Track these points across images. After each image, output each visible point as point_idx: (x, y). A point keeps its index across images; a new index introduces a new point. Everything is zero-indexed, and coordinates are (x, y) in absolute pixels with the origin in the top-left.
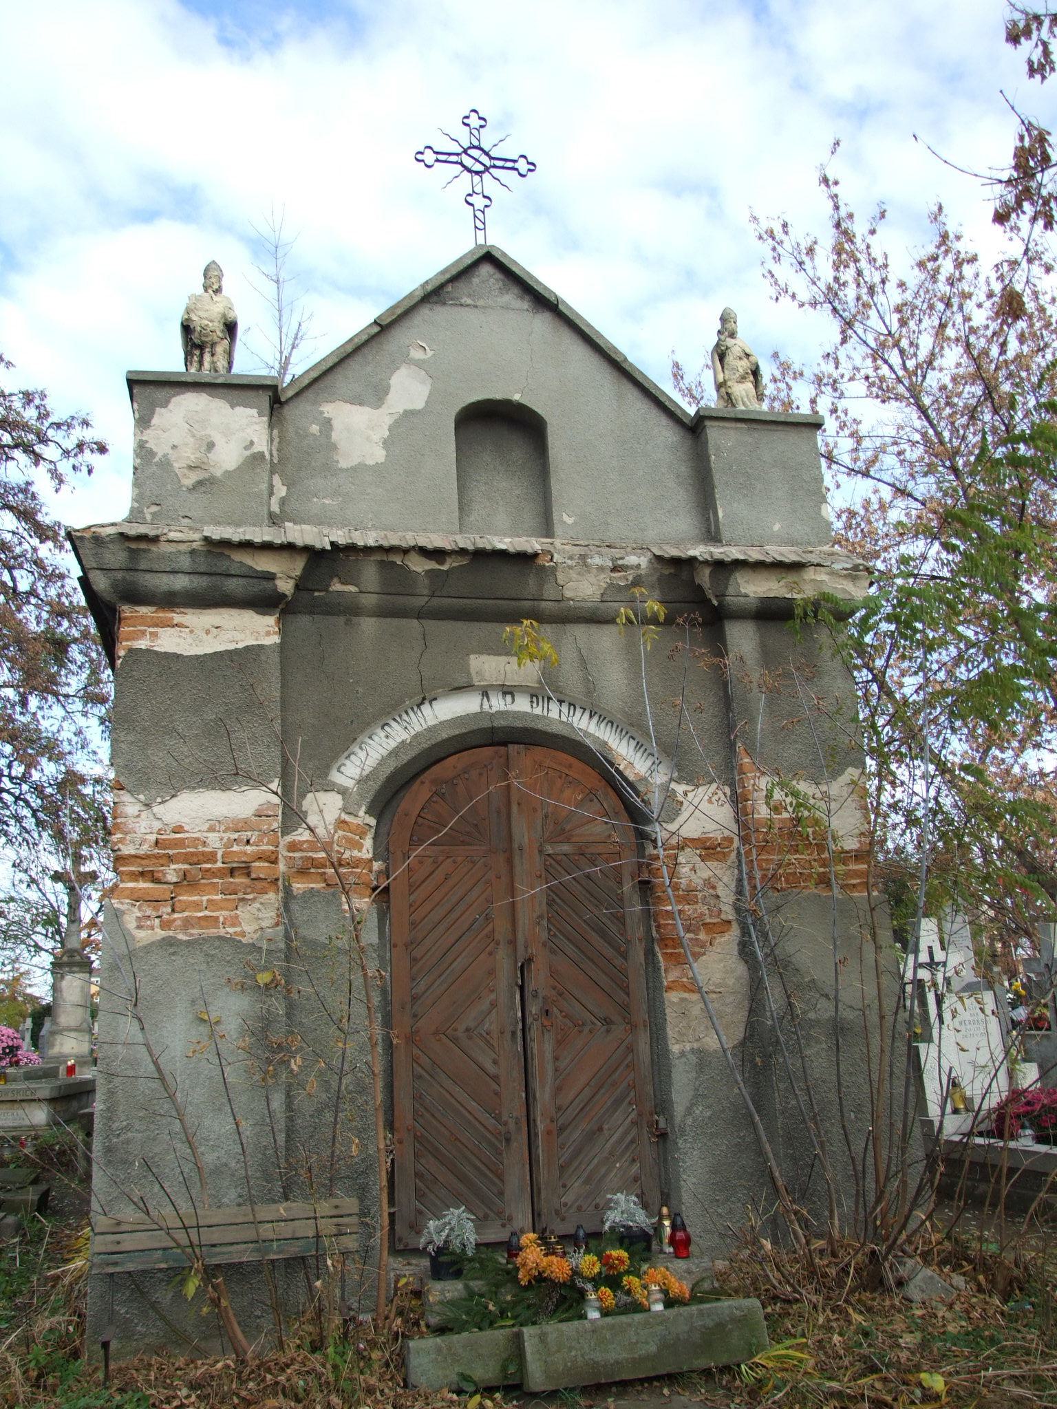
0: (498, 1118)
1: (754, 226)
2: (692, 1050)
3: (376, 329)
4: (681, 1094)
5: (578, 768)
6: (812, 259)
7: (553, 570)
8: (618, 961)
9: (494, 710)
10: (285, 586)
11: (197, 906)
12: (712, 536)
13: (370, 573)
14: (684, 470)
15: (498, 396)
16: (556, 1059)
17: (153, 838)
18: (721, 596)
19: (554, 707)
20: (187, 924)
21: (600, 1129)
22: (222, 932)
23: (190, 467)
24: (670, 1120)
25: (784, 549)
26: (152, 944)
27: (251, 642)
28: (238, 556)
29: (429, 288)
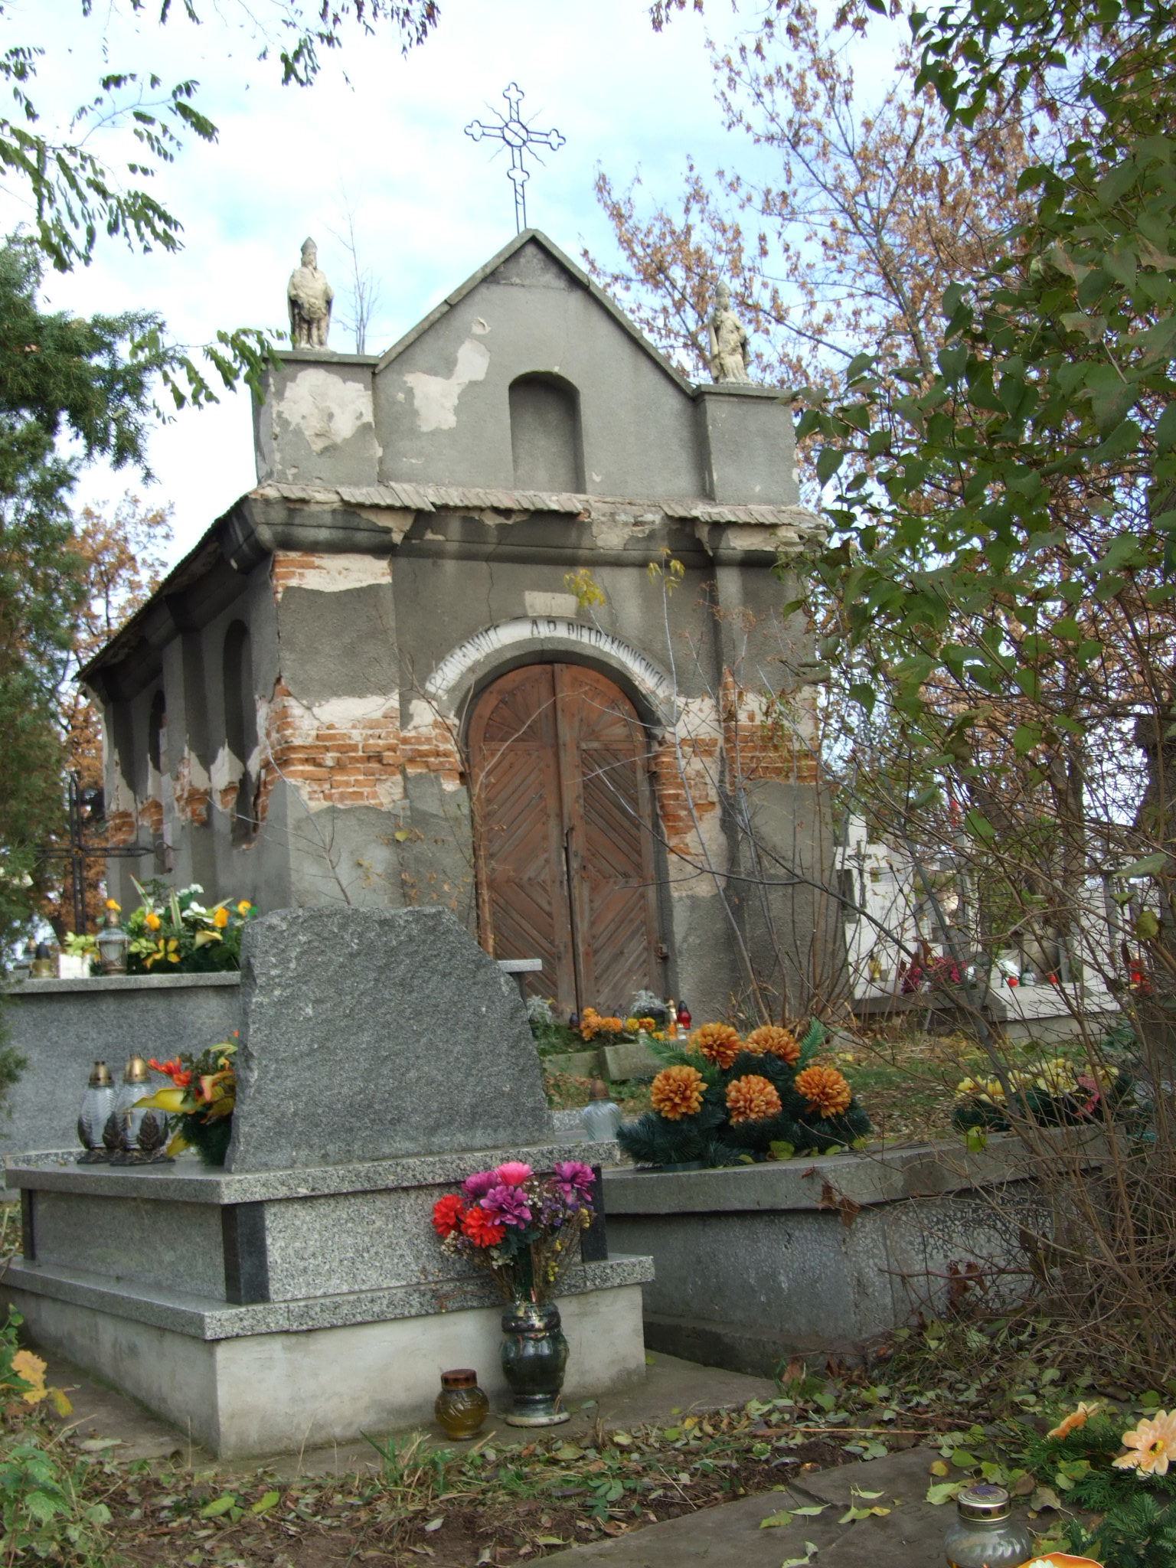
0: (552, 942)
1: (709, 51)
2: (688, 896)
3: (446, 308)
4: (679, 928)
5: (604, 684)
6: (771, 91)
7: (590, 524)
8: (634, 831)
9: (542, 636)
10: (397, 538)
11: (347, 784)
12: (707, 494)
13: (455, 527)
14: (685, 434)
15: (542, 368)
16: (591, 901)
17: (314, 733)
18: (715, 549)
19: (585, 632)
20: (343, 797)
21: (622, 953)
22: (366, 803)
23: (317, 435)
24: (671, 946)
25: (764, 508)
26: (321, 811)
27: (372, 582)
28: (367, 515)
29: (488, 271)
